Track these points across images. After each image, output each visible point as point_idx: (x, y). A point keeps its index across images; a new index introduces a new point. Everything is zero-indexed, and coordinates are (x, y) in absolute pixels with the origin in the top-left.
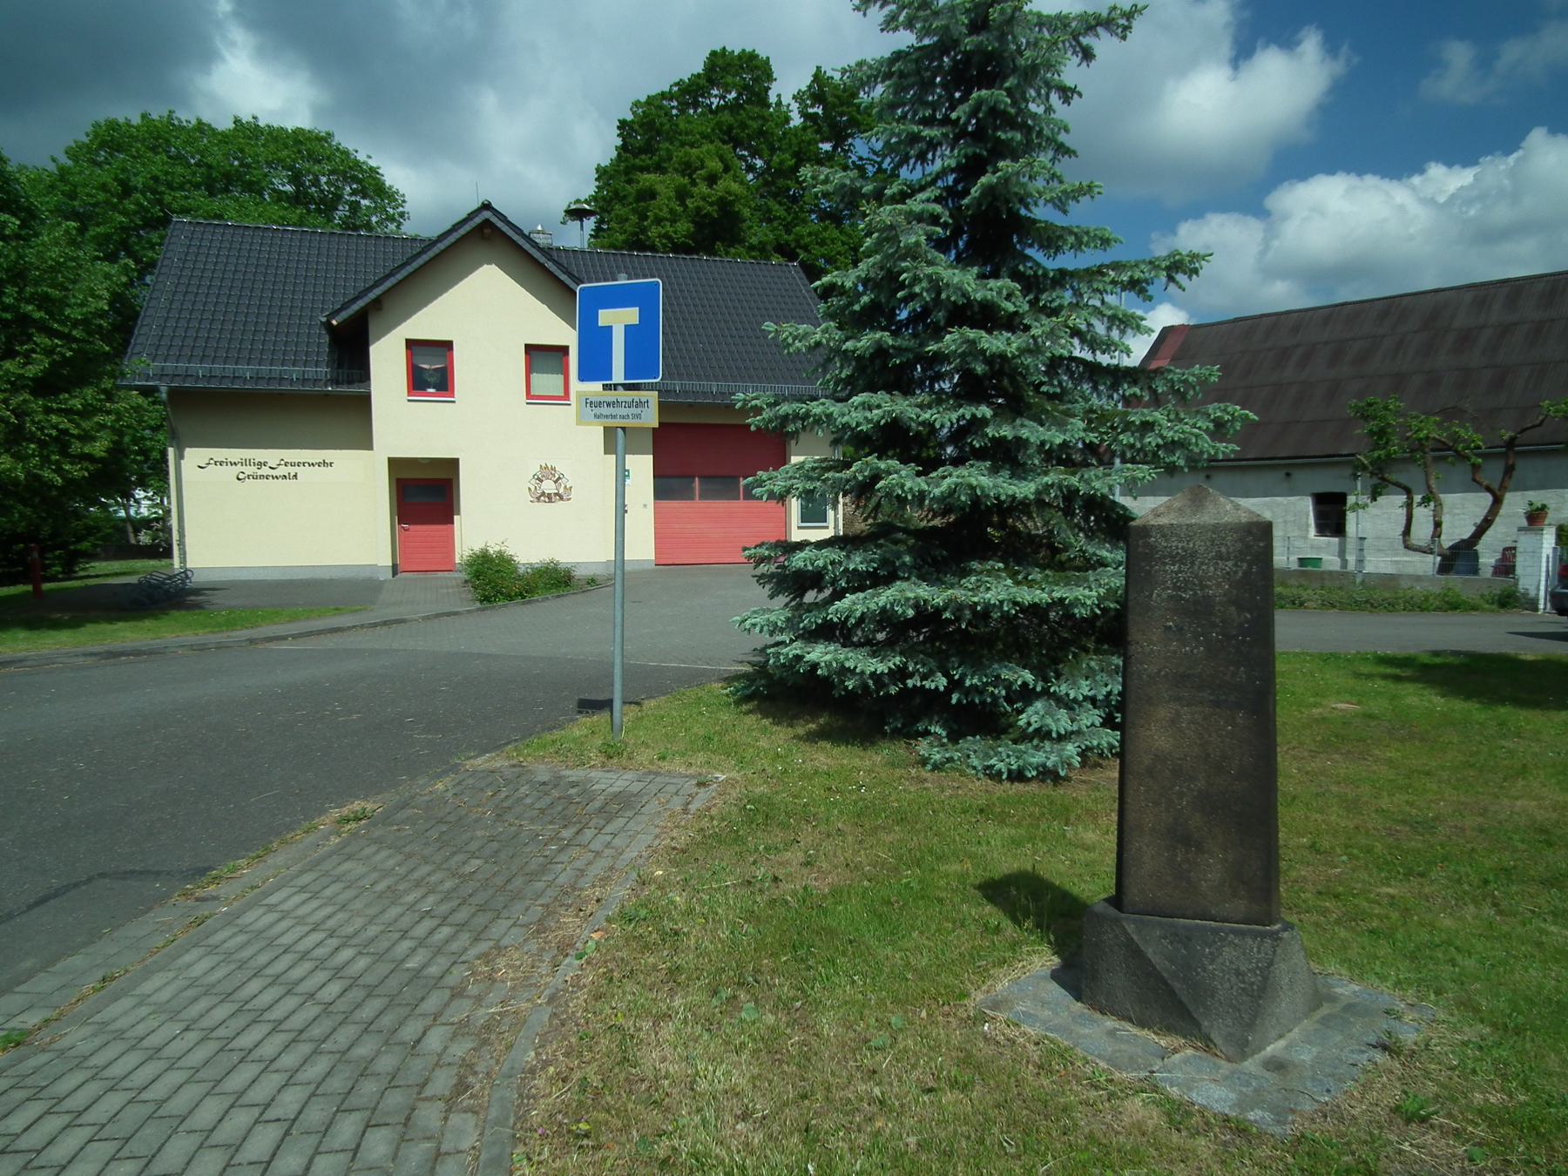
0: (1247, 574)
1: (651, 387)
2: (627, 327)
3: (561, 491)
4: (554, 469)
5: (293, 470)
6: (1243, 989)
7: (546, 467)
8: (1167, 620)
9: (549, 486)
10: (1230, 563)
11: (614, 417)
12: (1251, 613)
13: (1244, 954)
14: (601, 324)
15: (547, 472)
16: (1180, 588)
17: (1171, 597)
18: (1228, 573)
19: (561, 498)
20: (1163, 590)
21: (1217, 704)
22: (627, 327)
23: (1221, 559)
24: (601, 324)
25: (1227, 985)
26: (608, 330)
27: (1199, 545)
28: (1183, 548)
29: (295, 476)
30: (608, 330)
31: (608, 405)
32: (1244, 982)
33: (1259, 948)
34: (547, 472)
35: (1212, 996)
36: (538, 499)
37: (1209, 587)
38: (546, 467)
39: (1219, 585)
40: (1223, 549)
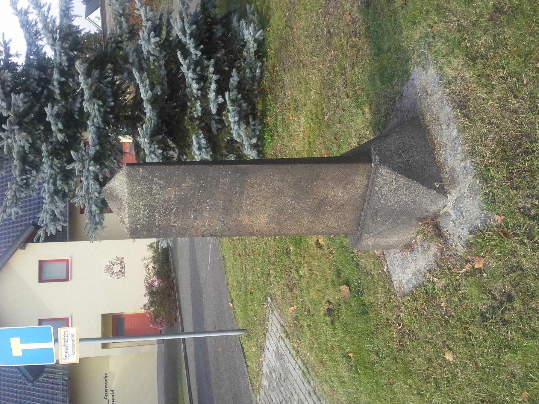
0: (161, 178)
1: (56, 333)
2: (22, 342)
3: (119, 262)
4: (107, 266)
5: (109, 393)
6: (407, 189)
7: (106, 270)
8: (190, 218)
9: (116, 268)
10: (154, 187)
11: (73, 346)
12: (187, 176)
13: (387, 184)
14: (21, 354)
15: (109, 269)
16: (169, 212)
17: (175, 217)
18: (160, 188)
19: (123, 262)
20: (171, 220)
21: (242, 193)
22: (22, 342)
23: (151, 191)
24: (21, 354)
25: (404, 196)
26: (24, 351)
27: (142, 203)
28: (144, 211)
29: (112, 391)
30: (24, 351)
31: (67, 349)
32: (403, 188)
33: (384, 176)
34: (109, 269)
35: (409, 205)
36: (123, 273)
37: (170, 197)
38: (106, 270)
39: (168, 193)
40: (145, 191)
